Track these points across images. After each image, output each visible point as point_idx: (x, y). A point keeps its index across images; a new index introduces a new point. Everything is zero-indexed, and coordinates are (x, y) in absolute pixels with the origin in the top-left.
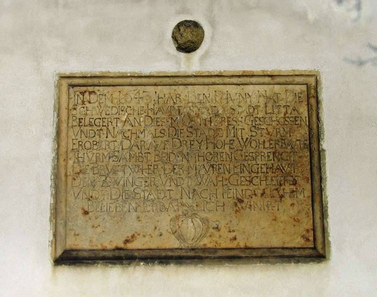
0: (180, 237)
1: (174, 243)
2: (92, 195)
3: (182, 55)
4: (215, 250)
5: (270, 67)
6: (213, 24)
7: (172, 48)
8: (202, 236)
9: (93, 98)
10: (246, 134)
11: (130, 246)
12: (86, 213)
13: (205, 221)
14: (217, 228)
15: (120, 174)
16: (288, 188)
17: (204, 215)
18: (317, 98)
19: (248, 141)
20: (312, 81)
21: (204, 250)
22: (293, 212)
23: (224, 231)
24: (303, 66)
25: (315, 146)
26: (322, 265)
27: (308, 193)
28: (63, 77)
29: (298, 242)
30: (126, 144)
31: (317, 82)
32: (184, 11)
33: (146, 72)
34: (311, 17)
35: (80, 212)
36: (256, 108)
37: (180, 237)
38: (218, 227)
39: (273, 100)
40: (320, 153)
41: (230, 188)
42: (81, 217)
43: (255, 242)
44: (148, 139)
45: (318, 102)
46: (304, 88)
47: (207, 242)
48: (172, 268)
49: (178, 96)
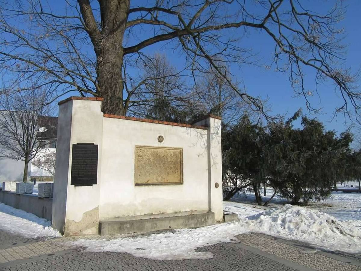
0: (158, 181)
1: (156, 182)
2: (317, 220)
3: (159, 143)
4: (164, 183)
5: (175, 146)
6: (165, 136)
7: (157, 141)
8: (161, 180)
9: (141, 151)
10: (170, 160)
11: (148, 182)
12: (140, 175)
13: (162, 177)
14: (164, 179)
15: (146, 167)
16: (177, 171)
17: (161, 176)
18: (182, 153)
19: (170, 161)
20: (181, 149)
21: (162, 183)
22: (177, 175)
23: (165, 179)
24: (180, 147)
25: (181, 162)
26: (182, 185)
27: (180, 172)
28: (136, 146)
29: (178, 181)
30: (148, 161)
31: (182, 150)
32: (160, 134)
33: (152, 146)
34: (182, 137)
35: (138, 175)
36: (172, 154)
37: (158, 181)
38: (248, 217)
39: (174, 153)
40: (183, 164)
41: (116, 261)
42: (139, 176)
43: (171, 181)
44: (152, 160)
45: (182, 154)
46: (180, 151)
47: (162, 181)
48: (157, 186)
49: (157, 151)
